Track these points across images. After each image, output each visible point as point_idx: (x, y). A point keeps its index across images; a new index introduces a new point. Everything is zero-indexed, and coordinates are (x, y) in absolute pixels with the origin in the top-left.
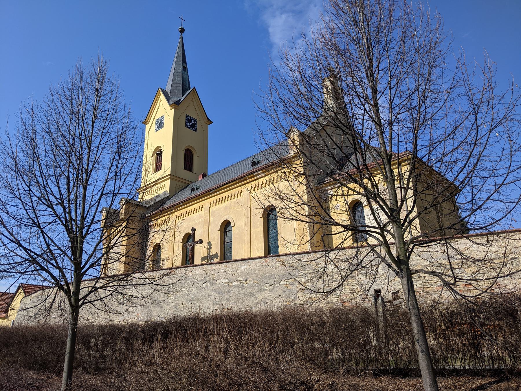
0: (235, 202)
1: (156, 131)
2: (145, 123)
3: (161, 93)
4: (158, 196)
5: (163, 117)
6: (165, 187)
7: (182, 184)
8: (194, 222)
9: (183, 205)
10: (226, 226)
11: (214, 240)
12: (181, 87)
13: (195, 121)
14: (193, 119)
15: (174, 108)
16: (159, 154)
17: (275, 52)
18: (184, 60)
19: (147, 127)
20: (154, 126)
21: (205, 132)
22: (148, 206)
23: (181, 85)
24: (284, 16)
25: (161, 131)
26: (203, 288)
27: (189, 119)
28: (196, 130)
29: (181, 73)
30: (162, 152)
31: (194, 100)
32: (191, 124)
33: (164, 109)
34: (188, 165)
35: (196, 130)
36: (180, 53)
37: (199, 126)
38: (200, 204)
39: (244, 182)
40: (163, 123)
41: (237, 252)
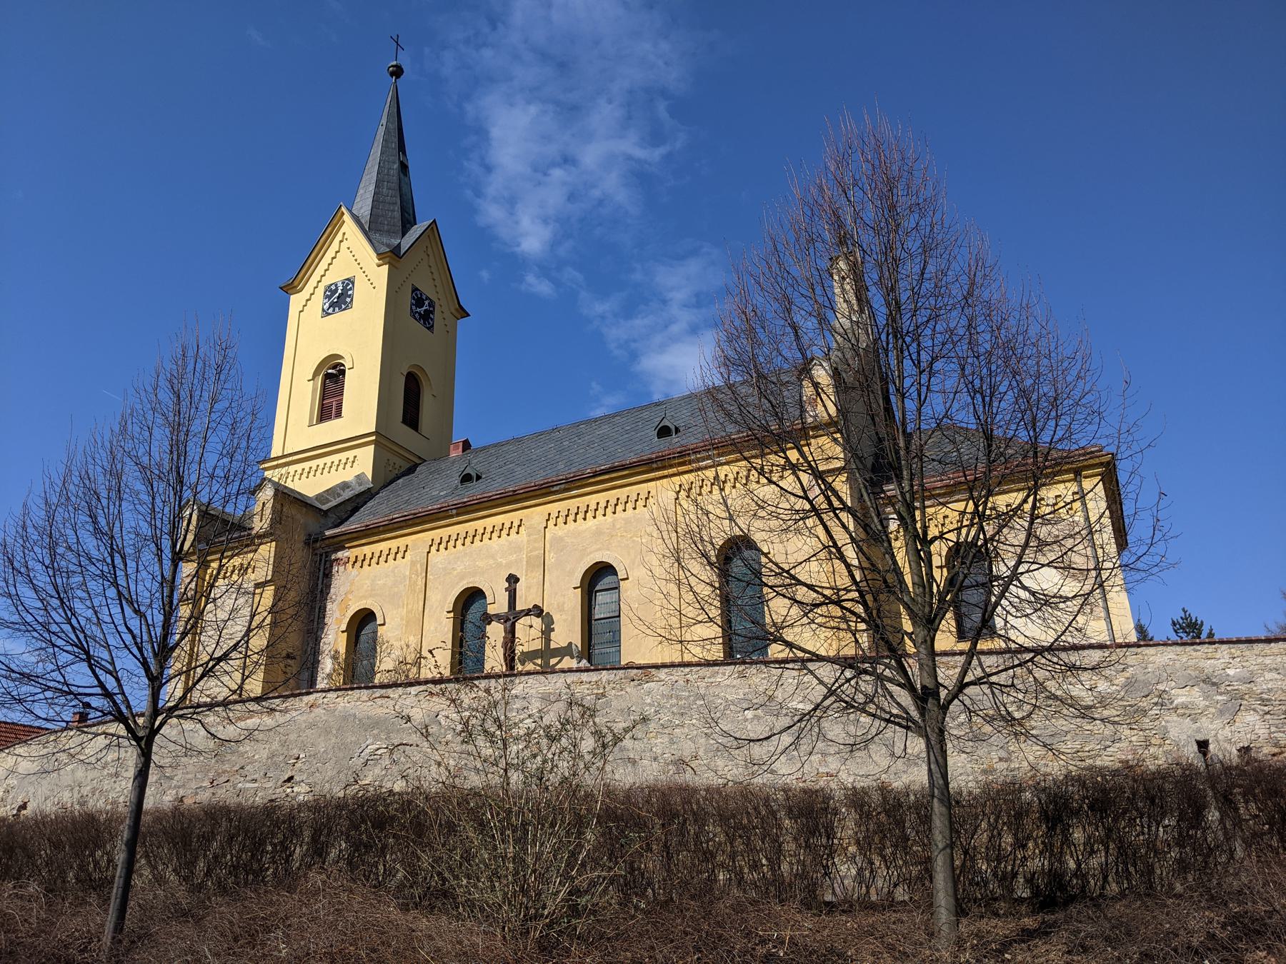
0: (627, 521)
1: (326, 313)
2: (290, 288)
3: (347, 217)
4: (345, 486)
5: (350, 282)
6: (362, 464)
7: (399, 462)
8: (491, 562)
10: (598, 577)
11: (561, 609)
12: (397, 214)
14: (427, 298)
15: (389, 263)
16: (332, 377)
17: (495, 185)
18: (402, 147)
19: (296, 301)
20: (319, 301)
21: (451, 335)
22: (325, 507)
23: (397, 208)
24: (533, 109)
25: (339, 317)
26: (746, 720)
28: (430, 328)
30: (343, 372)
32: (422, 310)
34: (411, 418)
35: (430, 328)
36: (394, 126)
37: (437, 317)
38: (515, 517)
39: (681, 469)
40: (351, 296)
41: (637, 646)
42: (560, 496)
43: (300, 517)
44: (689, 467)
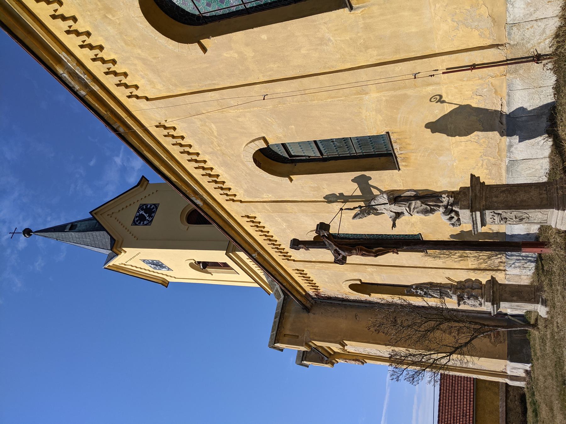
2: (165, 284)
3: (111, 263)
9: (256, 251)
10: (274, 160)
12: (97, 233)
13: (141, 208)
14: (138, 212)
15: (120, 247)
16: (205, 266)
22: (282, 296)
23: (94, 233)
27: (140, 220)
28: (156, 206)
29: (80, 234)
31: (110, 213)
32: (146, 215)
33: (132, 258)
35: (156, 206)
37: (149, 201)
38: (243, 222)
40: (153, 261)
42: (205, 196)
43: (291, 318)
44: (96, 88)
